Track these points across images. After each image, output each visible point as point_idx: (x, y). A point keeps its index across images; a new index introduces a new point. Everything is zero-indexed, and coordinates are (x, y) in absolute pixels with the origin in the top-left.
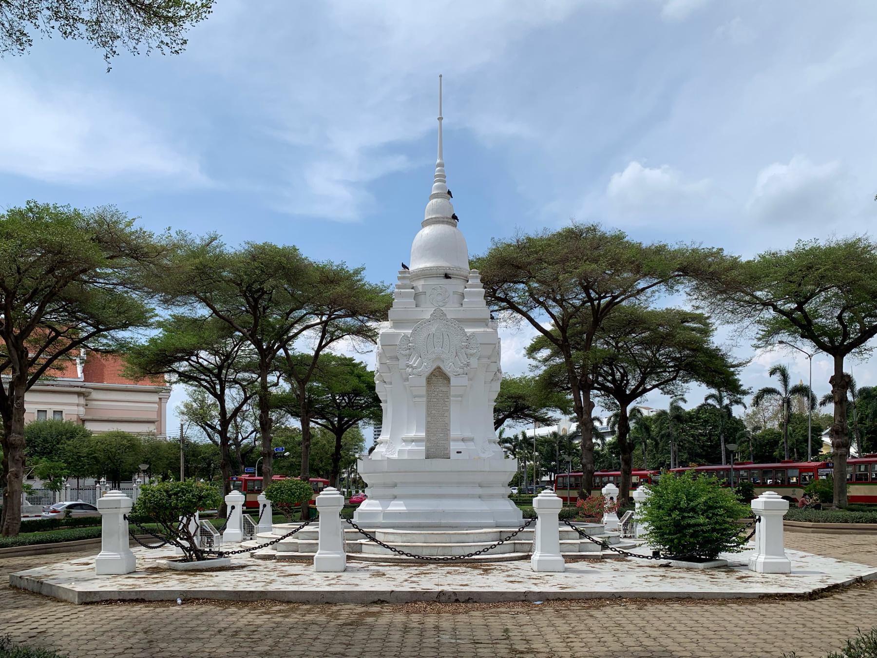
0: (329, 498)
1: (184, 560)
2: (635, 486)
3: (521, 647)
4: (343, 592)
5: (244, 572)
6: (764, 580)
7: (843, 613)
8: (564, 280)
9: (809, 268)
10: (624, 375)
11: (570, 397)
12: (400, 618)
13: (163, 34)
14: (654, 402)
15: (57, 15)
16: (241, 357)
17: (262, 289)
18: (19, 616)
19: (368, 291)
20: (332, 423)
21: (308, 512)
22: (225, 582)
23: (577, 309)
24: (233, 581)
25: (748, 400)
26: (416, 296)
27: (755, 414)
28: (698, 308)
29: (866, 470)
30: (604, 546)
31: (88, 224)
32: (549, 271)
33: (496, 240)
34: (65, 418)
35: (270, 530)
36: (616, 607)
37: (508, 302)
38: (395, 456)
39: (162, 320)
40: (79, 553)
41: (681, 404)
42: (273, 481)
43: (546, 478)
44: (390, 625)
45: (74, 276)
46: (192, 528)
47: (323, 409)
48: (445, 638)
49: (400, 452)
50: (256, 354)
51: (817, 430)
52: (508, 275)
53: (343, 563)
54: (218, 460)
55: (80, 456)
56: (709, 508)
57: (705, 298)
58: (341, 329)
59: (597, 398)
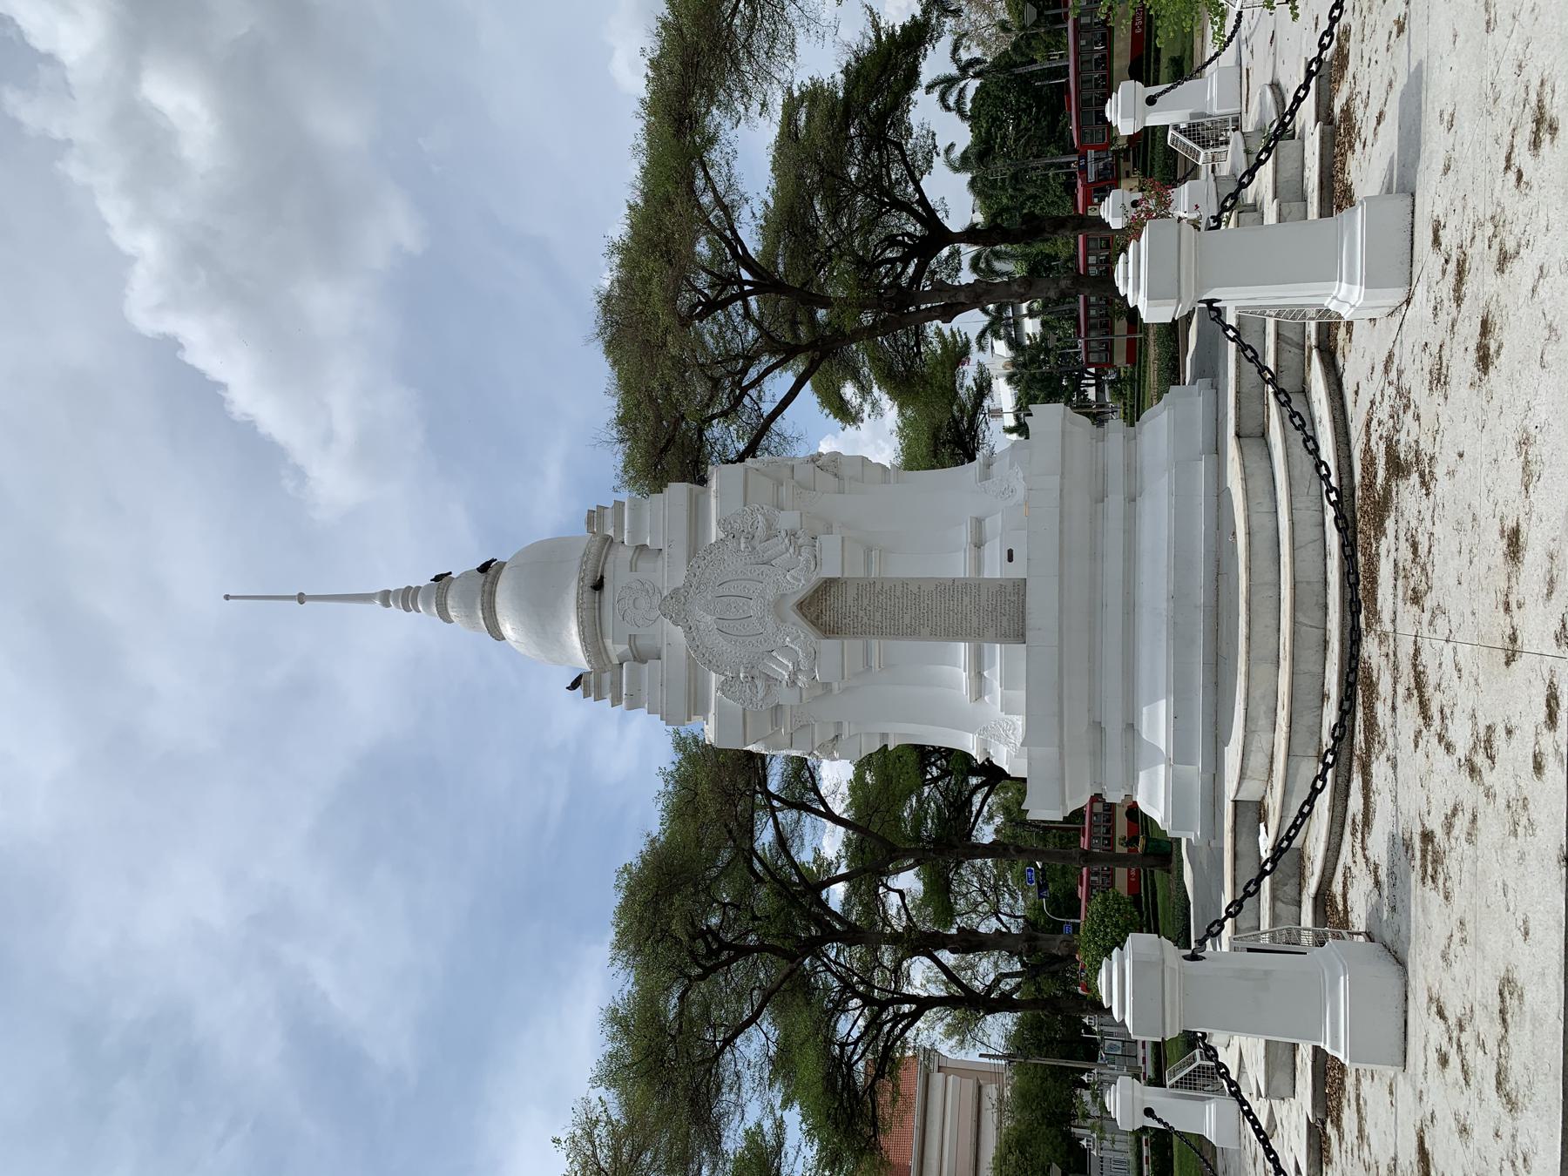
10: (891, 241)
14: (954, 199)
20: (978, 787)
26: (639, 657)
33: (617, 482)
38: (1019, 721)
41: (957, 153)
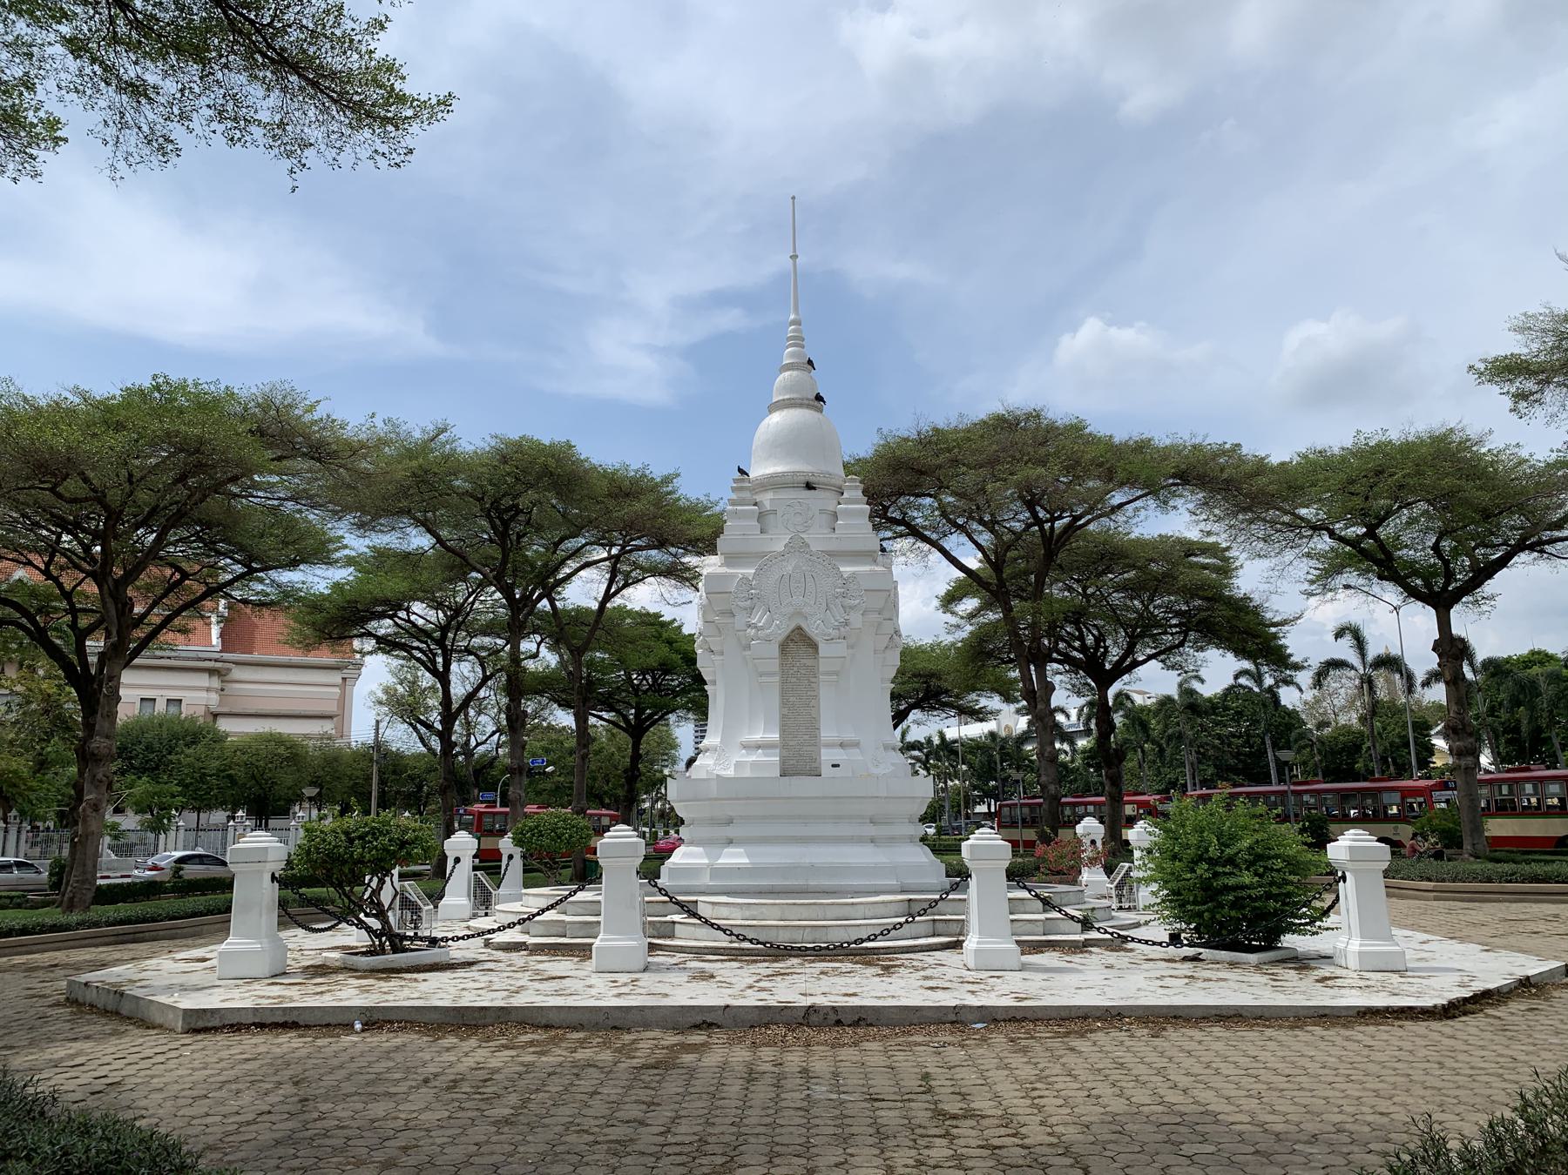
0: (620, 843)
1: (371, 952)
2: (1131, 821)
3: (953, 1107)
5: (472, 973)
6: (1362, 983)
9: (1379, 473)
10: (1100, 639)
11: (1015, 674)
12: (740, 1055)
13: (378, 141)
14: (1151, 683)
15: (221, 115)
16: (479, 612)
19: (685, 510)
20: (625, 718)
22: (439, 991)
23: (1017, 536)
24: (452, 990)
25: (1305, 678)
26: (761, 517)
27: (1317, 701)
28: (1209, 533)
29: (1511, 792)
32: (970, 478)
34: (186, 711)
35: (519, 899)
36: (1115, 1034)
37: (908, 525)
38: (730, 773)
40: (190, 941)
41: (1196, 685)
42: (526, 816)
44: (723, 1066)
45: (217, 488)
46: (386, 897)
47: (610, 694)
48: (820, 1091)
49: (738, 765)
50: (503, 606)
51: (1423, 728)
52: (907, 484)
53: (641, 957)
54: (435, 781)
56: (1258, 858)
57: (1219, 519)
58: (642, 568)
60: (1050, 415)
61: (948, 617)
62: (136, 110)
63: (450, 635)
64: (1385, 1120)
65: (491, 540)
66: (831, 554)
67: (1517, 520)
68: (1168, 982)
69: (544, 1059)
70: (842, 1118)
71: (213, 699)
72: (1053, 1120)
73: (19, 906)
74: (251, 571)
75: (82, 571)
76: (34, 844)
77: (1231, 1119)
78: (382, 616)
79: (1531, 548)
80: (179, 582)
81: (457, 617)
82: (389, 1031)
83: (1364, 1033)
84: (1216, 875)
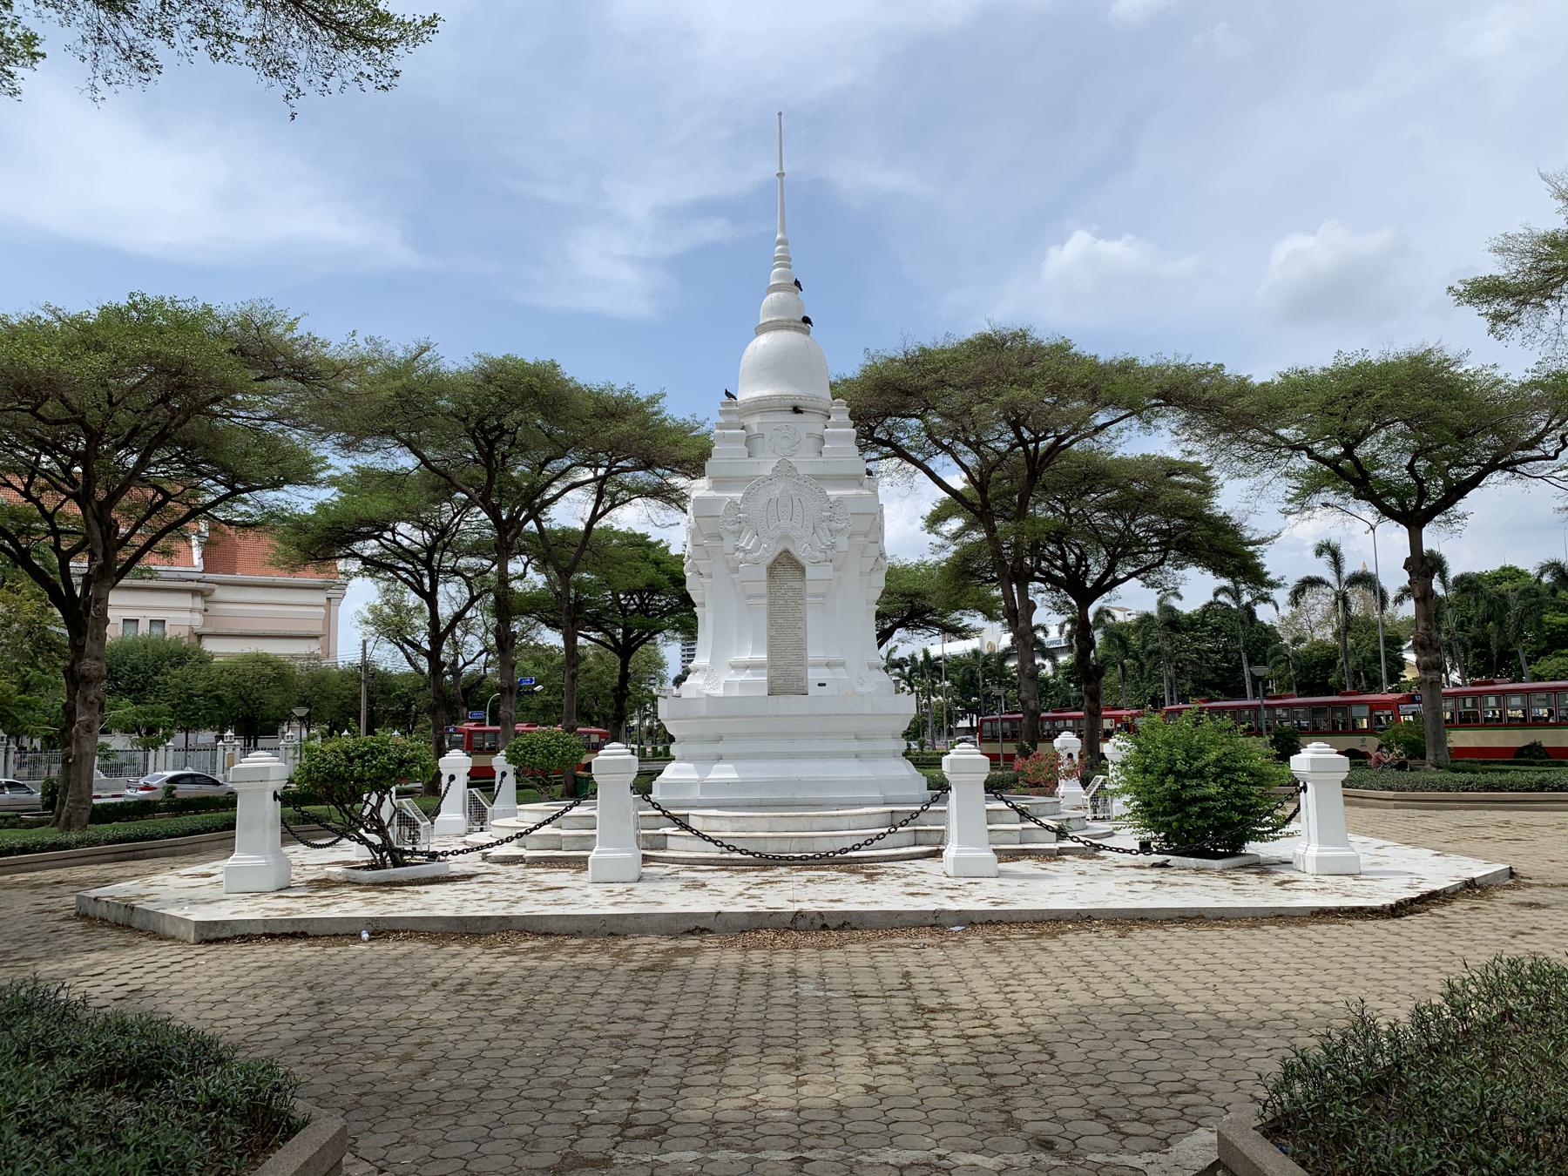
0: (614, 761)
1: (372, 867)
2: (1108, 735)
3: (932, 1002)
4: (637, 916)
5: (473, 885)
6: (1317, 886)
7: (1446, 937)
8: (979, 413)
9: (1357, 394)
10: (1081, 558)
11: (998, 593)
12: (732, 957)
13: (364, 63)
14: (1131, 600)
15: (202, 30)
16: (464, 532)
17: (500, 426)
18: (96, 964)
19: (670, 431)
20: (613, 637)
21: (576, 784)
22: (441, 902)
23: (1002, 456)
24: (454, 901)
25: (1281, 595)
26: (748, 440)
27: (1294, 617)
28: (1190, 453)
29: (1474, 704)
30: (1061, 833)
31: (225, 328)
32: (957, 399)
33: (872, 352)
34: (170, 632)
35: (512, 815)
36: (1084, 934)
37: (894, 446)
38: (719, 692)
39: (338, 474)
40: (189, 858)
42: (517, 734)
43: (964, 723)
44: (716, 969)
45: (200, 408)
46: (386, 813)
47: (598, 615)
48: (808, 989)
49: (727, 685)
50: (489, 527)
51: (1394, 642)
52: (892, 406)
53: (635, 867)
54: (424, 699)
55: (191, 696)
56: (1224, 770)
57: (1201, 439)
58: (628, 489)
59: (1040, 595)
60: (1036, 335)
61: (933, 538)
62: (116, 26)
63: (437, 556)
64: (1328, 1008)
65: (476, 461)
66: (815, 477)
67: (1491, 439)
68: (1136, 887)
69: (545, 963)
70: (828, 1014)
71: (197, 620)
72: (1022, 1013)
73: (13, 826)
74: (235, 492)
75: (62, 491)
76: (21, 765)
77: (1186, 1009)
78: (368, 536)
79: (1504, 467)
80: (162, 504)
81: (443, 538)
82: (395, 940)
83: (1315, 931)
84: (1184, 787)
